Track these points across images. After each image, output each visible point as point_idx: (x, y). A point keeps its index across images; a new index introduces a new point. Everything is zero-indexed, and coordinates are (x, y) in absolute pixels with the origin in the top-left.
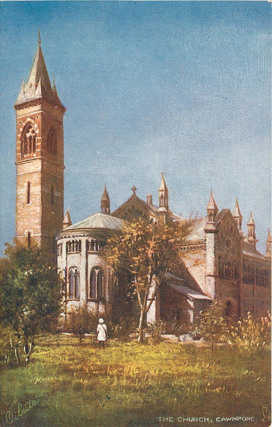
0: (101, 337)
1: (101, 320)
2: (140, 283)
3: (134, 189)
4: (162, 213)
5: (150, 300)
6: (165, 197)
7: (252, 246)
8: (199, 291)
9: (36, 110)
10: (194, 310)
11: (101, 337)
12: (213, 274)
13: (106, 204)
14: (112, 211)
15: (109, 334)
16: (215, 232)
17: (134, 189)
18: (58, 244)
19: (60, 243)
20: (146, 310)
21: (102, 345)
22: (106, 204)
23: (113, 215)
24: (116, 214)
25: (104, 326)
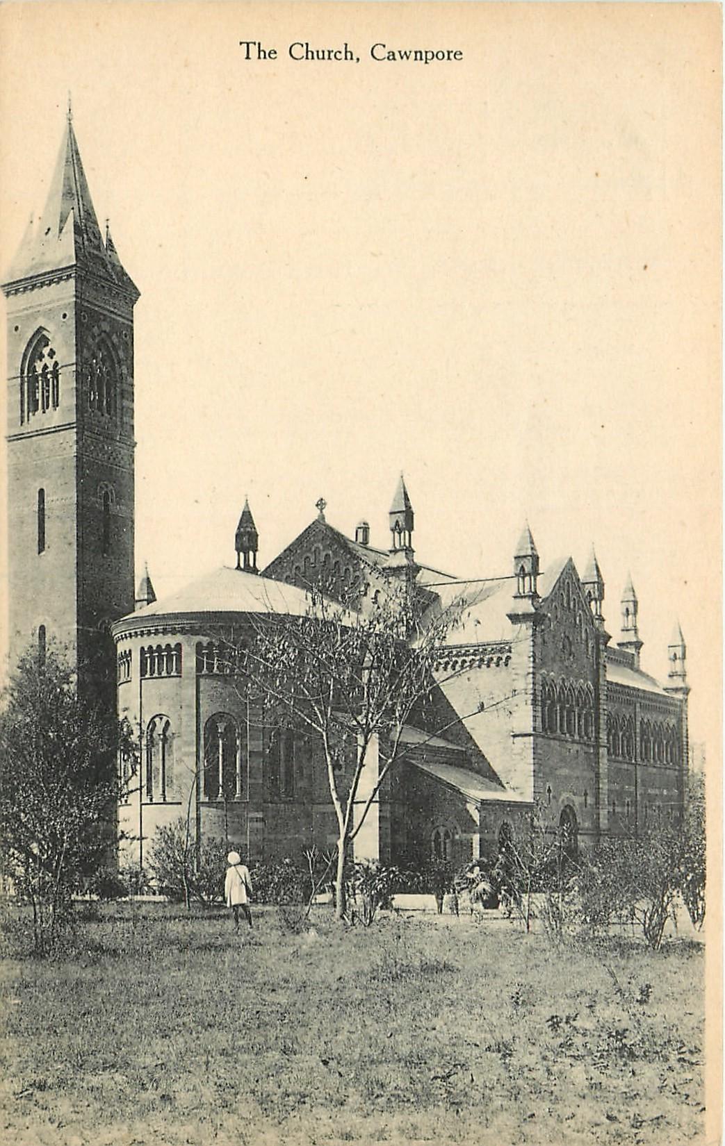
0: (236, 893)
1: (234, 857)
2: (108, 331)
3: (321, 504)
4: (396, 571)
5: (368, 668)
6: (405, 520)
7: (627, 658)
8: (492, 777)
9: (66, 291)
10: (222, 787)
11: (236, 893)
12: (530, 731)
13: (247, 538)
14: (262, 565)
15: (257, 891)
16: (536, 619)
17: (321, 504)
18: (119, 652)
19: (125, 651)
20: (351, 835)
21: (242, 913)
22: (247, 538)
23: (267, 574)
24: (275, 571)
25: (243, 869)
